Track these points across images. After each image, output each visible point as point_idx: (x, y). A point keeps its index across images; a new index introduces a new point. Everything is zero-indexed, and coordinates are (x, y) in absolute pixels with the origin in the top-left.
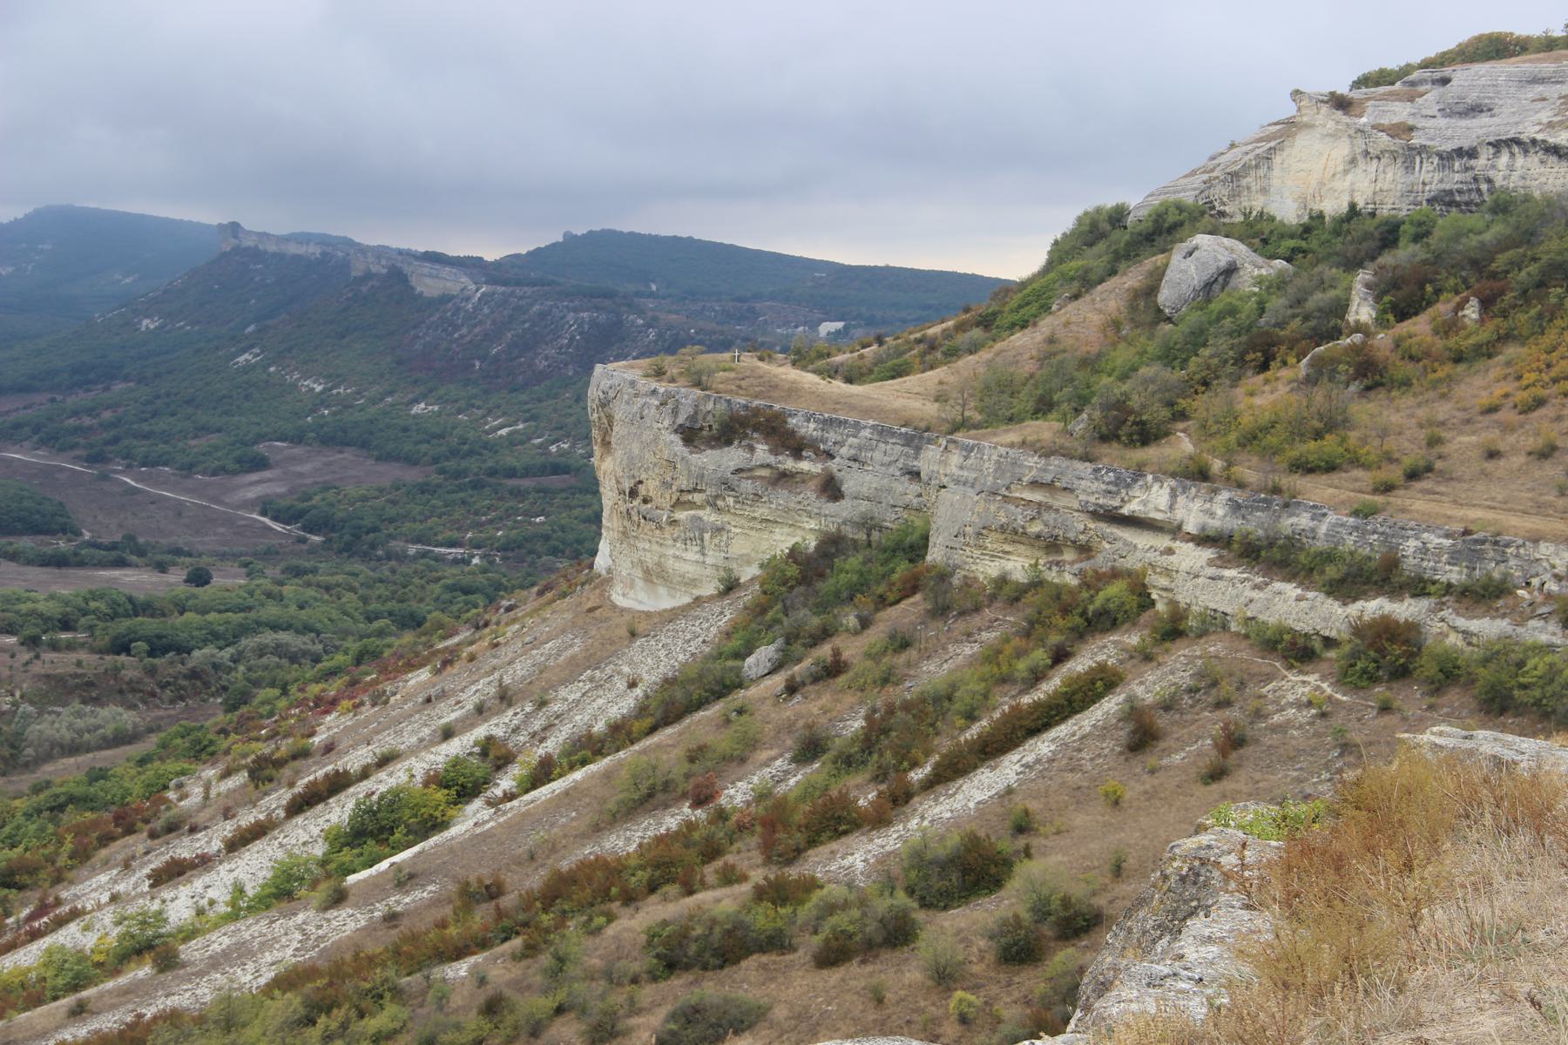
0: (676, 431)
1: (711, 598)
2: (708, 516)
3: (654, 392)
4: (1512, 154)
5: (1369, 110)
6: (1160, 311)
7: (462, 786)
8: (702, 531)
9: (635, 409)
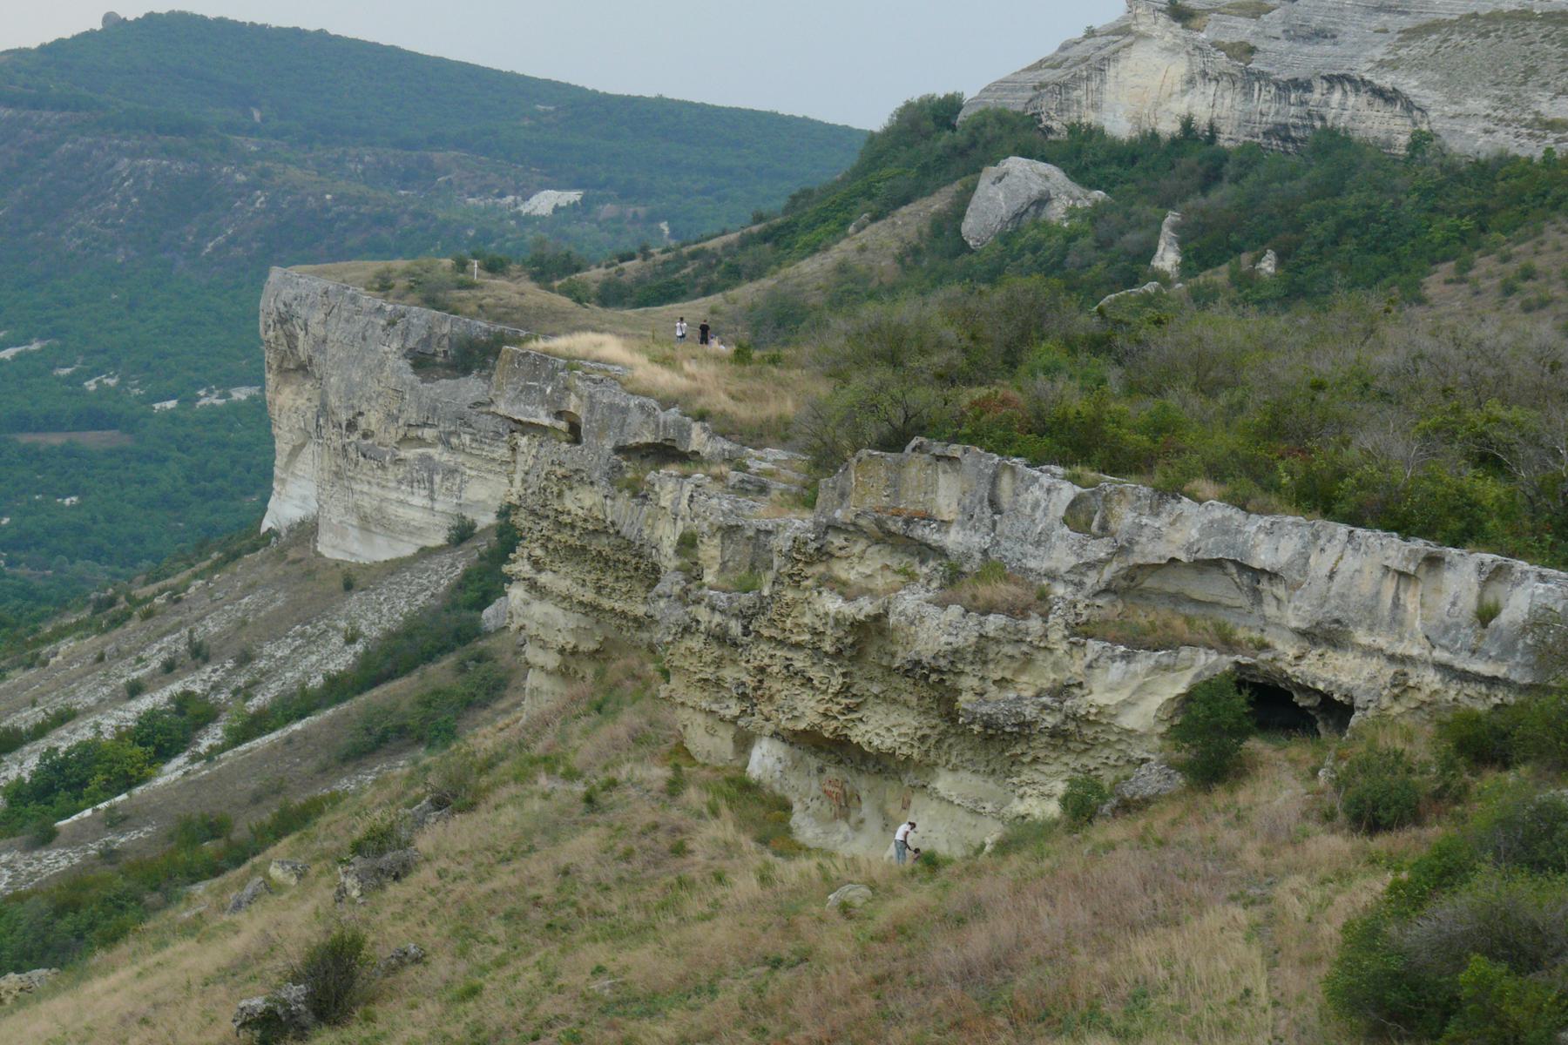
0: (405, 356)
1: (439, 550)
2: (439, 454)
3: (380, 310)
4: (1345, 92)
5: (1210, 25)
6: (965, 243)
7: (161, 739)
8: (432, 471)
9: (357, 328)
